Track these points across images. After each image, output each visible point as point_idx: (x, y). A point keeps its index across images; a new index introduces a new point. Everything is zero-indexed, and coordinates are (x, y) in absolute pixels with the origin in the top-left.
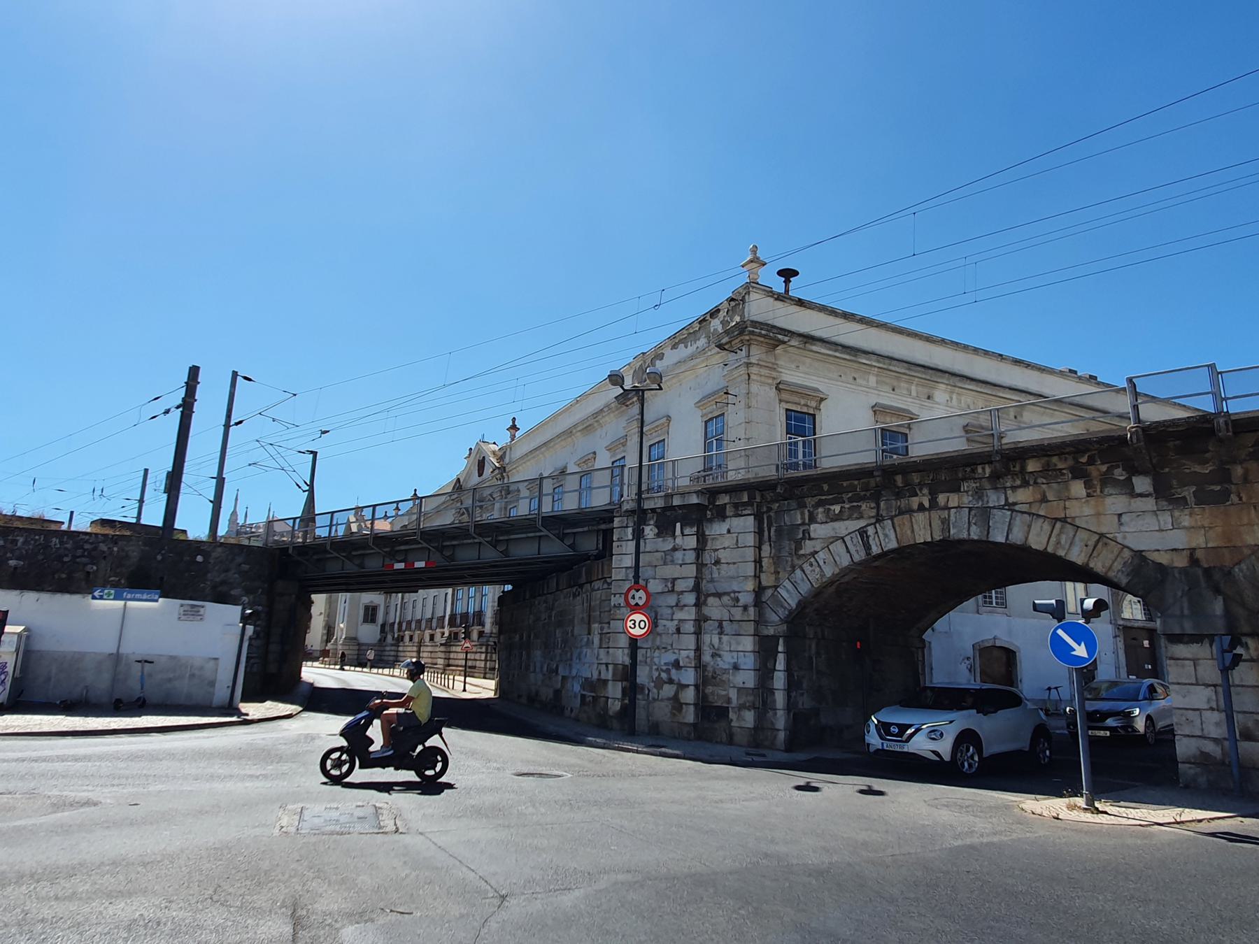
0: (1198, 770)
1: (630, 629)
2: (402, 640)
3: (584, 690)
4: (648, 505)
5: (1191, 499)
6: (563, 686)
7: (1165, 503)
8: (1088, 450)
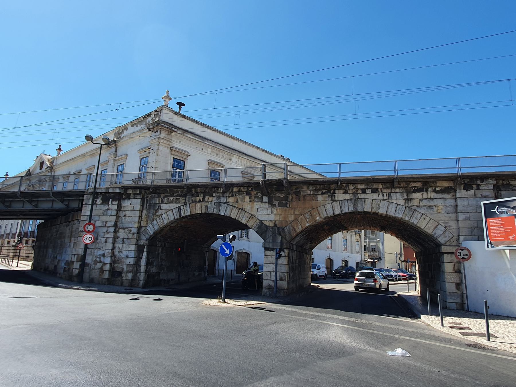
0: (268, 290)
1: (85, 241)
3: (65, 265)
4: (99, 191)
5: (277, 205)
6: (58, 263)
7: (270, 206)
8: (251, 186)
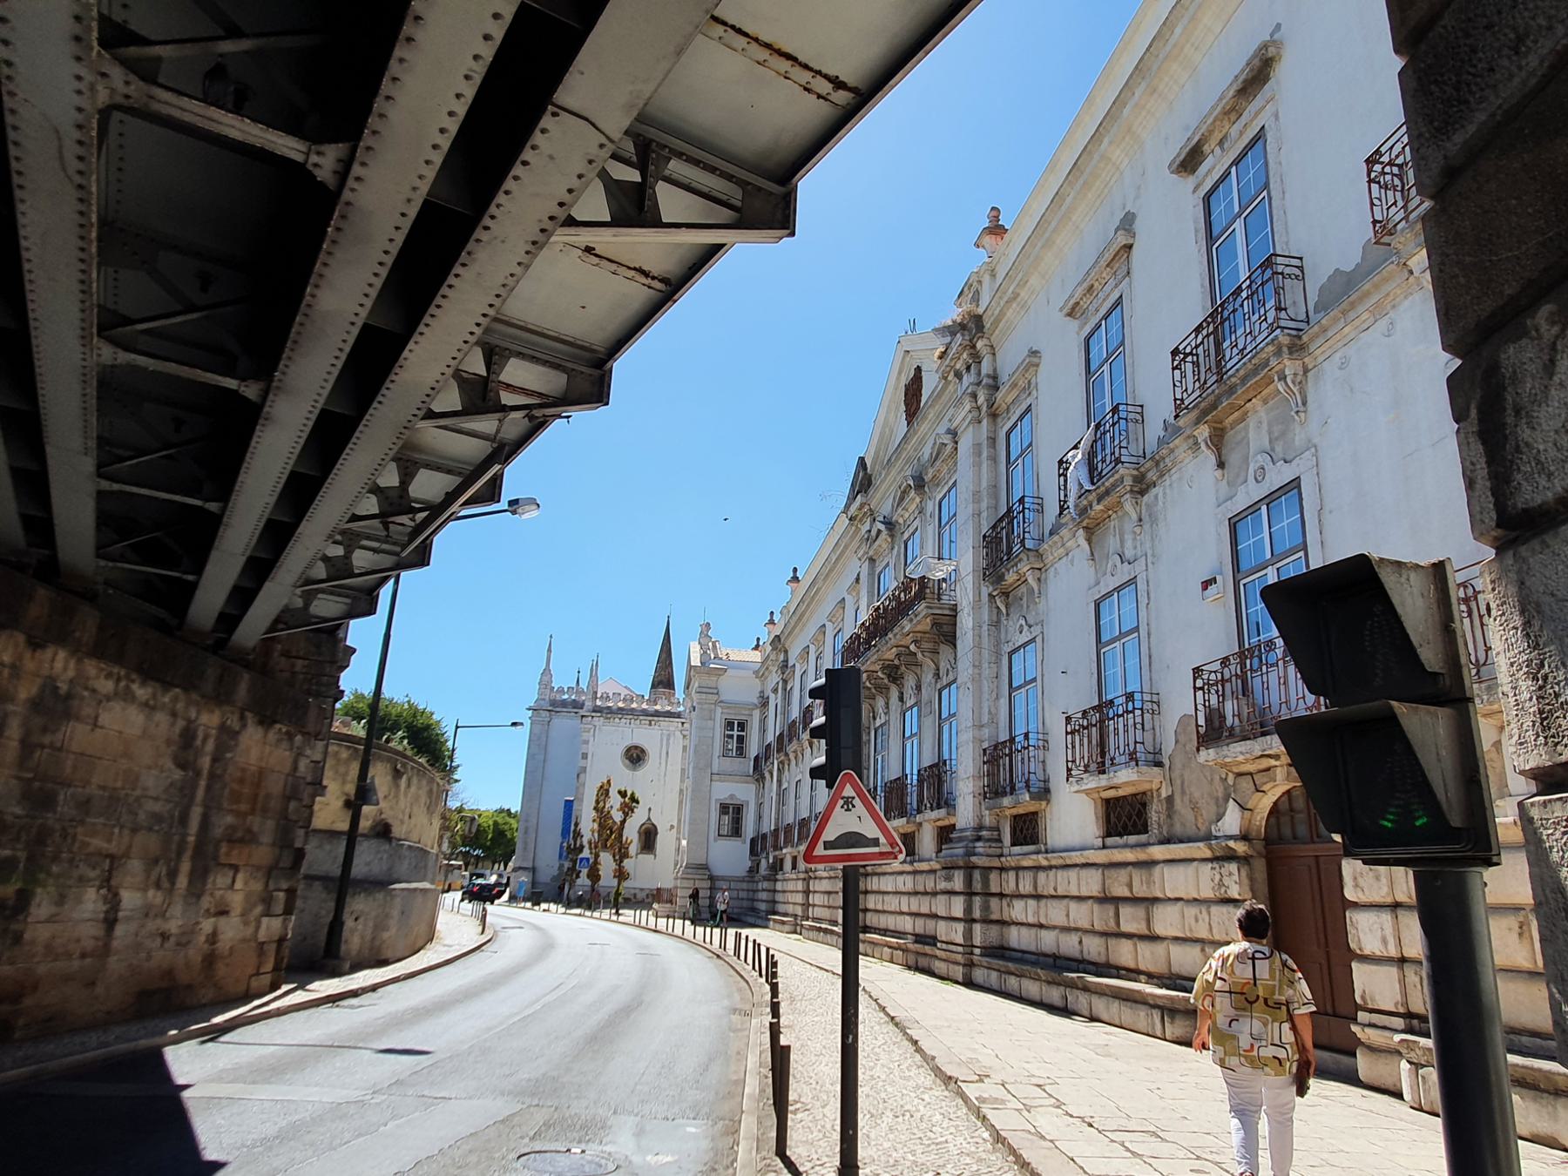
2: (781, 869)
